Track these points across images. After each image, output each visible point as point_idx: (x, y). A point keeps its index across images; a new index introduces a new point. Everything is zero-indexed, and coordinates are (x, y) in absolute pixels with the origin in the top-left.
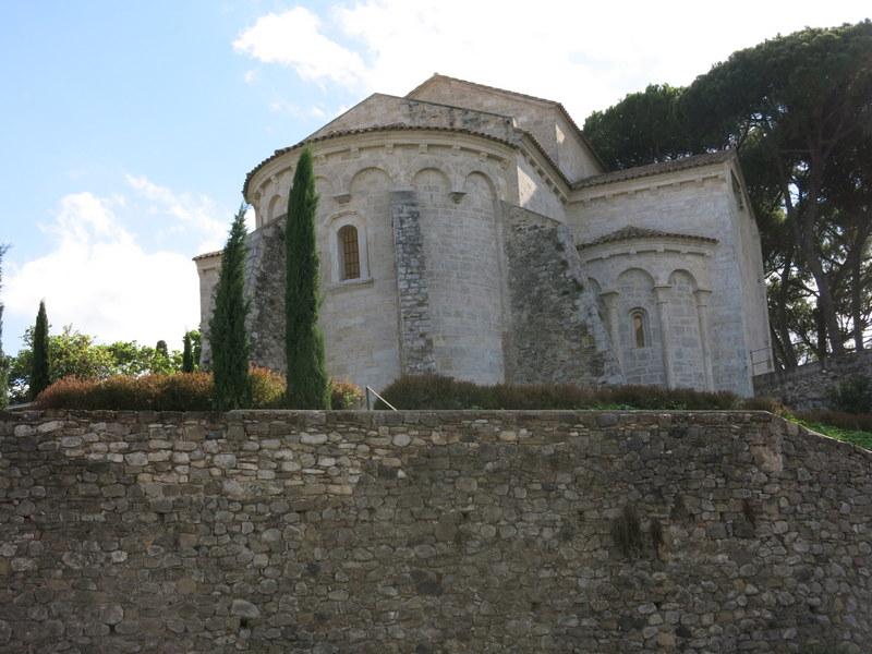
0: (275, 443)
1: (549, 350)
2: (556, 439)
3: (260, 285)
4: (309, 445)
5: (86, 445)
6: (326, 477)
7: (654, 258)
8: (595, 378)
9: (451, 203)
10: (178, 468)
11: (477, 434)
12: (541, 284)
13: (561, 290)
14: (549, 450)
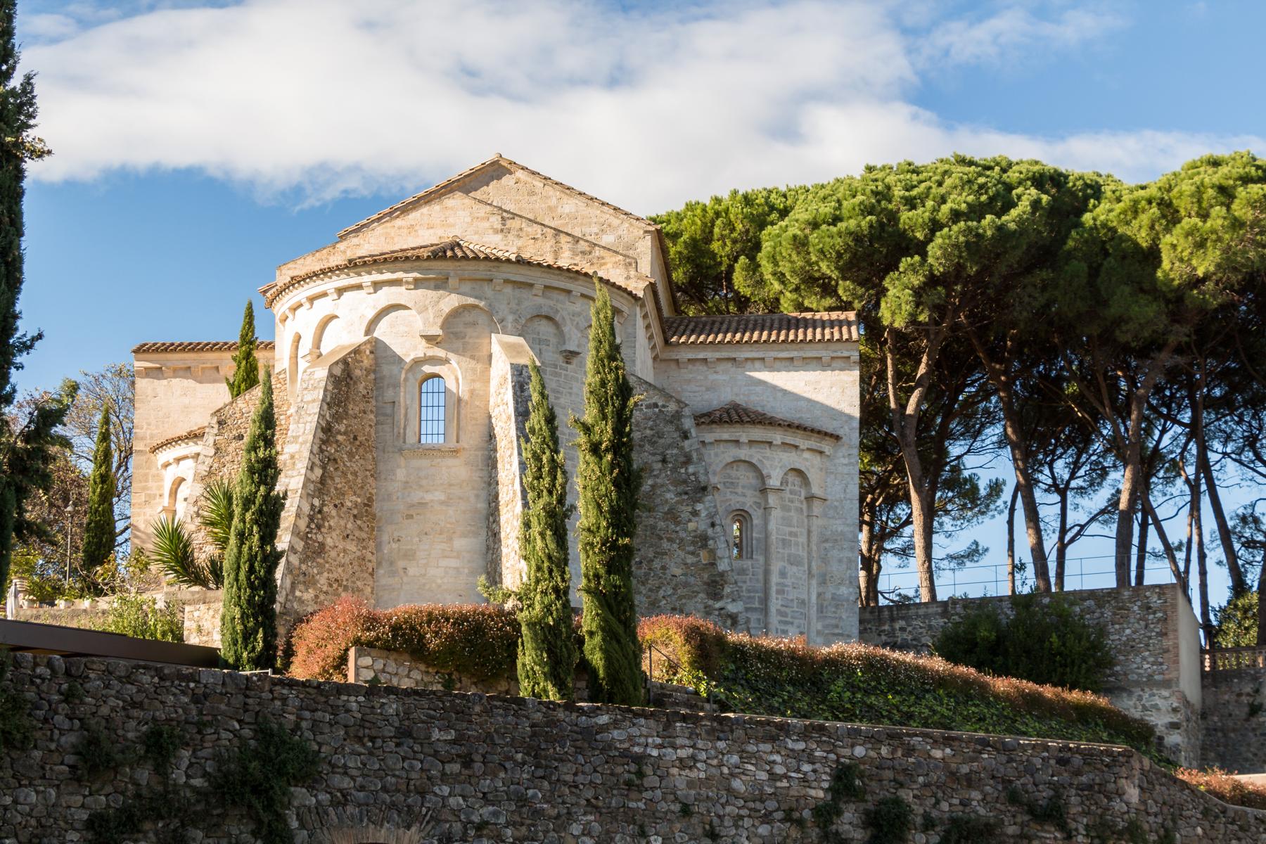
0: (767, 747)
1: (657, 561)
2: (973, 760)
3: (325, 438)
4: (792, 750)
5: (630, 738)
6: (804, 780)
7: (768, 452)
8: (711, 602)
10: (699, 765)
11: (914, 750)
12: (657, 476)
13: (680, 489)
14: (965, 769)
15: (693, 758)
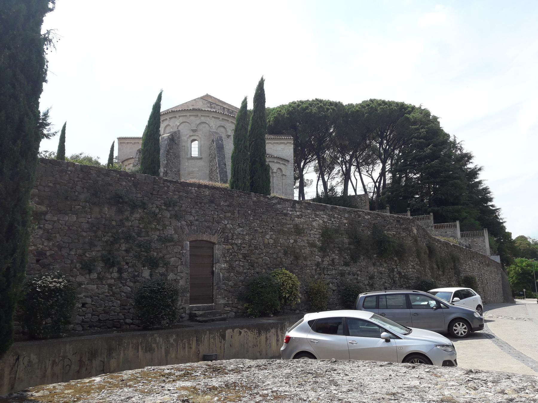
0: (322, 213)
7: (273, 164)
9: (226, 138)
15: (301, 215)
